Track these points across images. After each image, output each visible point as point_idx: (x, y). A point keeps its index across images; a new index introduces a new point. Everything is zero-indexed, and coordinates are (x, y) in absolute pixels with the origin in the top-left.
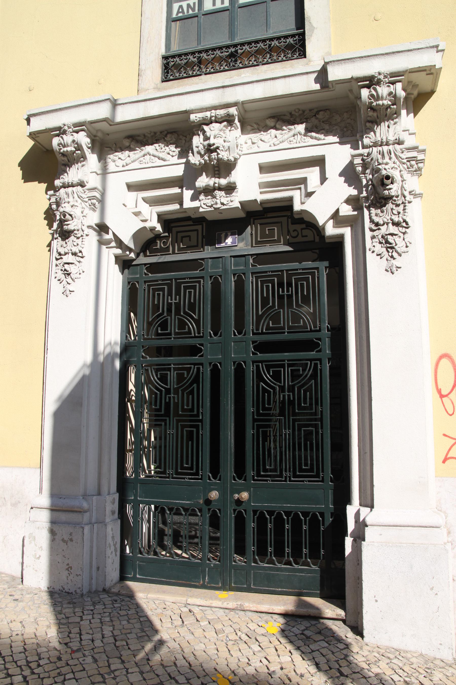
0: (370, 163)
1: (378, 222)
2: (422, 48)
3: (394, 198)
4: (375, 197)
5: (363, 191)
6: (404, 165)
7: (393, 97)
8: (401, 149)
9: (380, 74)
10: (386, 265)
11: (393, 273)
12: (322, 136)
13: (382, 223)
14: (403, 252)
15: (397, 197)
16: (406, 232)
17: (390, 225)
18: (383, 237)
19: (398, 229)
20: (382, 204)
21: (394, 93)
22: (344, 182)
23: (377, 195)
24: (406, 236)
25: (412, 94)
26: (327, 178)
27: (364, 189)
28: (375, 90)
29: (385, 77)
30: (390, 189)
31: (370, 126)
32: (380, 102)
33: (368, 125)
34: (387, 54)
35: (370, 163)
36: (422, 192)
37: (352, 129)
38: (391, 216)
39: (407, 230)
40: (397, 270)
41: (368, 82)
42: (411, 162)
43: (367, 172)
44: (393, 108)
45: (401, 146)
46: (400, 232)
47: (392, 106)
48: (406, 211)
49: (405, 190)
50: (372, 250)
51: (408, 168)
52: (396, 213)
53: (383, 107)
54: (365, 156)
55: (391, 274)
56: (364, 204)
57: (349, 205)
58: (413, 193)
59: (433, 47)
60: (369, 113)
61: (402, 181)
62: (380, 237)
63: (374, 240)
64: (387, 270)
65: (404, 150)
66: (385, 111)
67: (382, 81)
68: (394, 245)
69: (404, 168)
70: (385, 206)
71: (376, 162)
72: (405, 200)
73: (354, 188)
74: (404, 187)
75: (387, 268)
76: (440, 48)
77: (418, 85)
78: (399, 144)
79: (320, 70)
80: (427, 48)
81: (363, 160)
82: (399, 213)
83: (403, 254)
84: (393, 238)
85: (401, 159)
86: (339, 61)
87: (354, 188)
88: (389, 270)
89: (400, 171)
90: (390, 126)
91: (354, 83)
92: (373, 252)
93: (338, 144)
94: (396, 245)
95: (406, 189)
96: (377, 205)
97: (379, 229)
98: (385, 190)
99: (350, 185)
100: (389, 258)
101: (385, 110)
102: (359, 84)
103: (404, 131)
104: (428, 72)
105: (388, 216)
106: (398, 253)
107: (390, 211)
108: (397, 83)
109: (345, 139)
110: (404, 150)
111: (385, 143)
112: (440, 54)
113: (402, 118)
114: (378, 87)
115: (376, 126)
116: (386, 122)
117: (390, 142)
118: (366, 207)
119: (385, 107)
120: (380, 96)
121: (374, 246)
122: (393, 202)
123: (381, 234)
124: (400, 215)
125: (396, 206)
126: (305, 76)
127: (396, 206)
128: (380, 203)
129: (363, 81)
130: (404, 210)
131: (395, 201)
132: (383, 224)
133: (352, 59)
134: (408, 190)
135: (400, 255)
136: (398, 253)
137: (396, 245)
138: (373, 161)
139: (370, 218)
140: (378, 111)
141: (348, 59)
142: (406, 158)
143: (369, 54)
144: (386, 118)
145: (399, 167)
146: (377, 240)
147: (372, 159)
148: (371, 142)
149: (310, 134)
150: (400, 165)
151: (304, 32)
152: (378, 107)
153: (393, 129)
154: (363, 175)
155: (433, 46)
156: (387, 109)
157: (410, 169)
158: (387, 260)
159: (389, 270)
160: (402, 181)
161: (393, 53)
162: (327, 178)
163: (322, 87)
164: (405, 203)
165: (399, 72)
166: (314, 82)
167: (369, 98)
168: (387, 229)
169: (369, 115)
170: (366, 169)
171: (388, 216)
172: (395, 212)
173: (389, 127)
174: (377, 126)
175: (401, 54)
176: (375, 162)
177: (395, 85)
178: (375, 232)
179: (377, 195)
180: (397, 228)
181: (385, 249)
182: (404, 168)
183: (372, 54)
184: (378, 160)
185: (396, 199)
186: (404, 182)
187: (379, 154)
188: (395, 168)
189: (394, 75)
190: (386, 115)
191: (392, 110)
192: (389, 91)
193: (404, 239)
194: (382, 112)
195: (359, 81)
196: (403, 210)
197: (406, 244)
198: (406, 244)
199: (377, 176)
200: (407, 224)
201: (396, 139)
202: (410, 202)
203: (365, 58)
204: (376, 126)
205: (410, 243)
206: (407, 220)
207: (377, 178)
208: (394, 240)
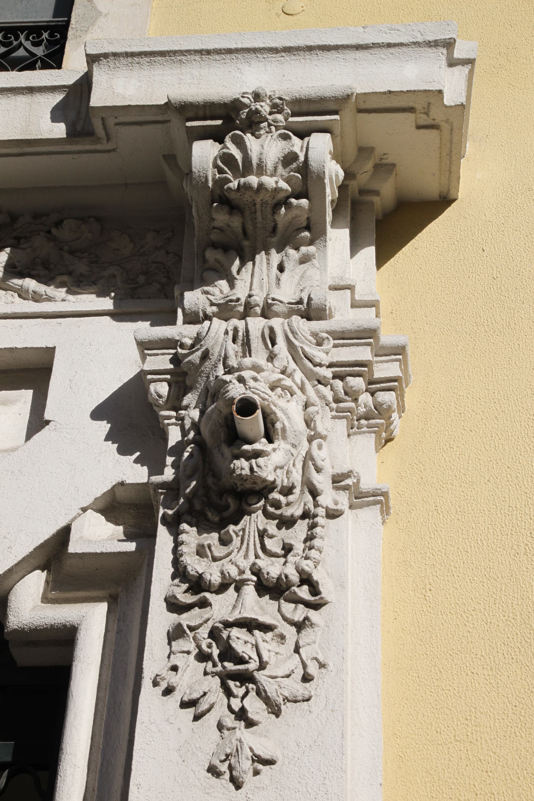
0: (197, 368)
1: (200, 577)
2: (401, 45)
3: (275, 495)
4: (202, 485)
5: (164, 465)
6: (320, 386)
7: (298, 170)
8: (315, 335)
9: (257, 97)
10: (212, 748)
11: (237, 784)
12: (61, 292)
13: (216, 579)
14: (286, 699)
15: (288, 491)
16: (306, 618)
17: (249, 590)
18: (214, 634)
19: (279, 610)
20: (226, 514)
21: (302, 158)
22: (107, 439)
23: (210, 481)
24: (307, 635)
25: (377, 193)
26: (48, 422)
27: (170, 460)
28: (240, 144)
29: (276, 108)
30: (257, 454)
31: (217, 261)
32: (253, 180)
33: (211, 255)
34: (288, 50)
35: (197, 368)
36: (383, 486)
37: (164, 280)
38: (257, 557)
39: (312, 614)
40: (256, 773)
41: (219, 122)
42: (349, 379)
43: (185, 402)
44: (299, 207)
45: (316, 325)
46: (285, 619)
47: (293, 200)
48: (316, 542)
49: (318, 470)
50: (164, 685)
51: (337, 400)
52: (279, 550)
53: (261, 196)
54: (182, 346)
55: (231, 786)
56: (161, 511)
57: (117, 524)
58: (349, 482)
59: (435, 44)
60: (215, 216)
61: (310, 440)
62: (204, 632)
63: (179, 645)
64: (213, 771)
65: (325, 335)
66: (270, 216)
67: (266, 120)
68: (253, 666)
69: (323, 397)
70: (236, 523)
71: (221, 366)
72: (316, 505)
73: (136, 461)
74: (313, 459)
75: (217, 763)
76: (457, 54)
77: (394, 165)
78: (309, 319)
79: (75, 84)
80: (416, 44)
81: (176, 360)
82: (288, 549)
83: (286, 709)
84: (252, 640)
85: (310, 365)
86: (132, 55)
87: (136, 461)
88: (224, 767)
89: (306, 406)
90: (288, 266)
91: (175, 121)
92: (168, 691)
93: (108, 318)
94: (262, 666)
95: (319, 463)
96: (209, 514)
97: (204, 604)
98: (237, 457)
99: (123, 451)
100: (229, 720)
101: (269, 209)
102: (189, 124)
103: (335, 288)
104: (423, 120)
105: (246, 556)
106: (267, 700)
107: (253, 538)
108: (314, 135)
109: (132, 306)
110: (325, 335)
111: (258, 310)
112: (462, 71)
113: (329, 244)
114: (248, 138)
115: (237, 262)
116: (273, 251)
117: (275, 308)
118: (165, 521)
119: (271, 202)
120: (255, 161)
121: (175, 668)
122: (271, 509)
123: (210, 624)
124: (290, 557)
125: (279, 527)
126: (22, 100)
127: (279, 527)
128: (220, 509)
129: (204, 119)
130: (310, 538)
131: (277, 505)
132: (222, 588)
133: (175, 53)
134: (329, 471)
135: (276, 711)
136: (267, 700)
137: (262, 666)
138: (208, 364)
139: (176, 562)
140: (247, 212)
141: (162, 54)
142: (331, 366)
143: (233, 46)
144: (274, 239)
145: (302, 389)
146: (191, 646)
147: (205, 356)
148: (212, 304)
149: (17, 282)
150: (308, 386)
151: (68, 22)
152: (247, 196)
153: (297, 277)
154: (173, 413)
155: (436, 41)
156: (277, 206)
157: (342, 405)
158: (220, 727)
159: (224, 767)
160: (310, 440)
161: (310, 49)
162: (48, 422)
163: (72, 133)
164: (315, 516)
165: (322, 100)
166: (49, 116)
167: (215, 166)
168: (234, 607)
169: (216, 224)
170: (186, 390)
171: (246, 556)
172: (272, 545)
173: (281, 268)
174: (243, 263)
175: (333, 54)
176: (215, 366)
177: (306, 139)
178: (185, 615)
179: (210, 481)
180: (276, 603)
181: (217, 680)
182: (323, 397)
183: (240, 46)
184: (226, 358)
185: (283, 499)
186: (315, 443)
187: (234, 341)
188: (284, 388)
189: (305, 108)
190: (274, 229)
191: (294, 212)
192: (286, 151)
193: (297, 650)
194: (259, 219)
195: (190, 114)
196: (305, 541)
197: (304, 666)
198: (304, 666)
199: (213, 410)
200: (314, 590)
201: (300, 302)
202: (332, 515)
203: (217, 57)
204: (237, 262)
205: (322, 666)
206: (316, 577)
207: (215, 416)
208: (257, 647)
